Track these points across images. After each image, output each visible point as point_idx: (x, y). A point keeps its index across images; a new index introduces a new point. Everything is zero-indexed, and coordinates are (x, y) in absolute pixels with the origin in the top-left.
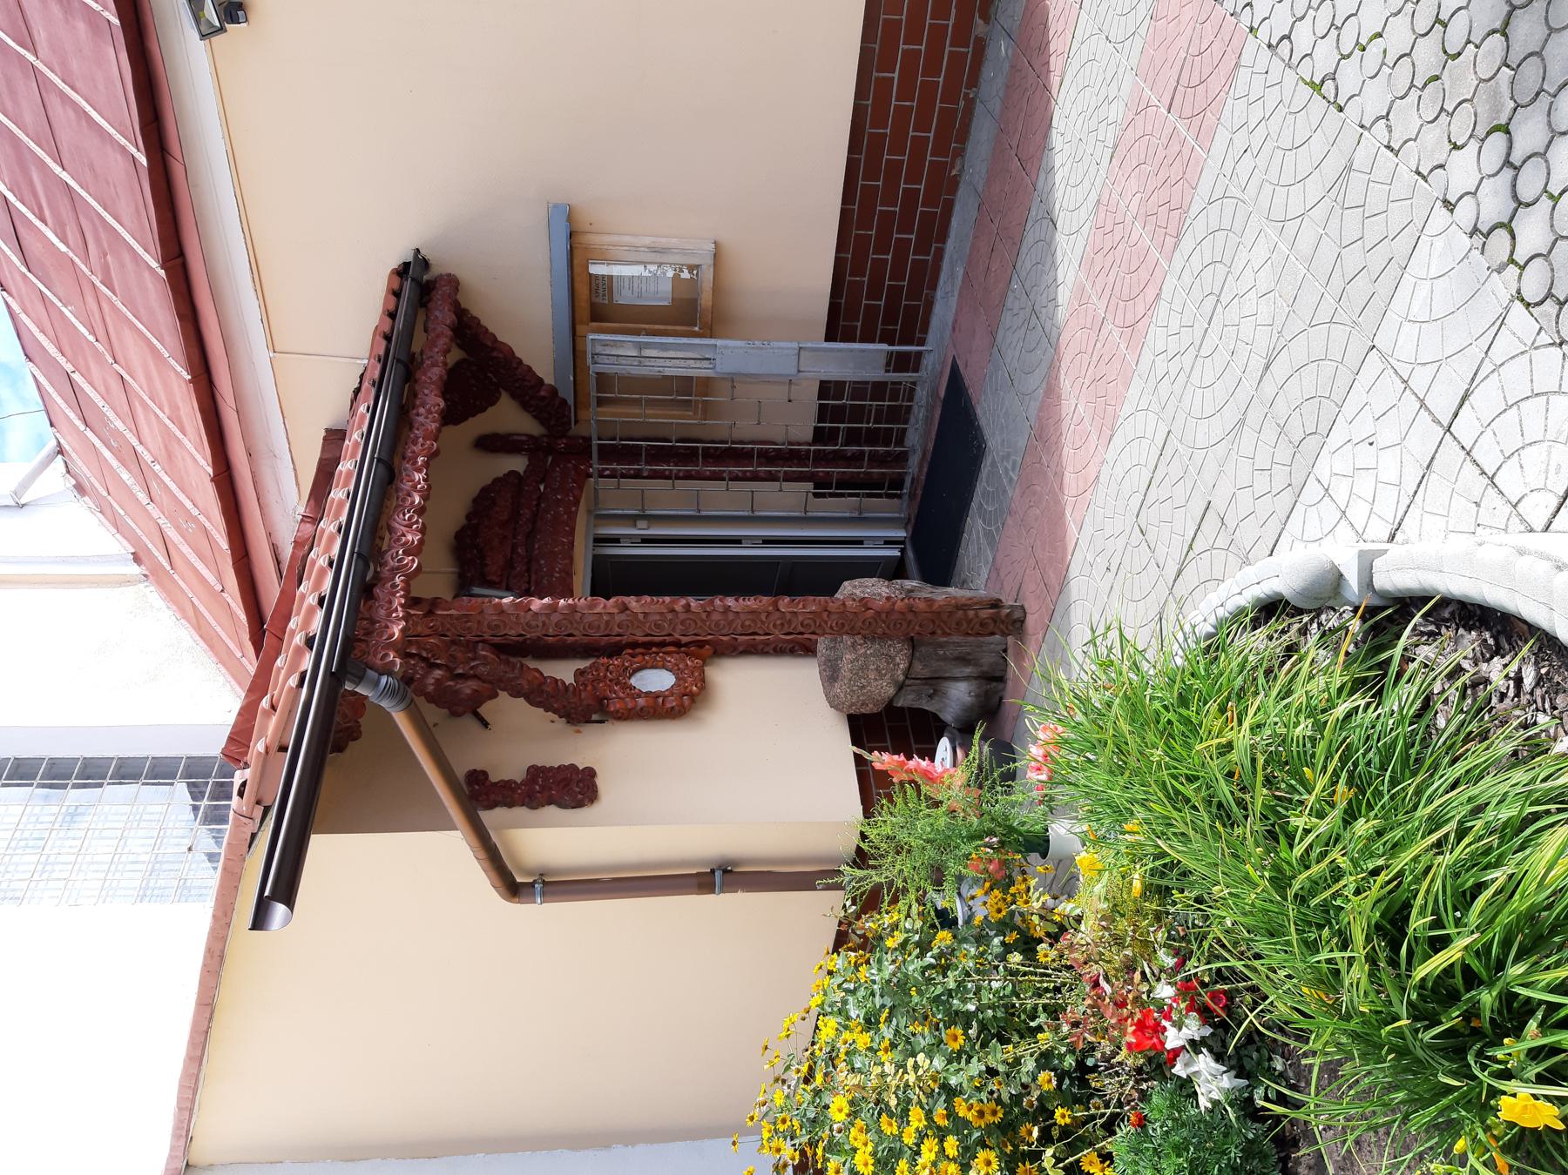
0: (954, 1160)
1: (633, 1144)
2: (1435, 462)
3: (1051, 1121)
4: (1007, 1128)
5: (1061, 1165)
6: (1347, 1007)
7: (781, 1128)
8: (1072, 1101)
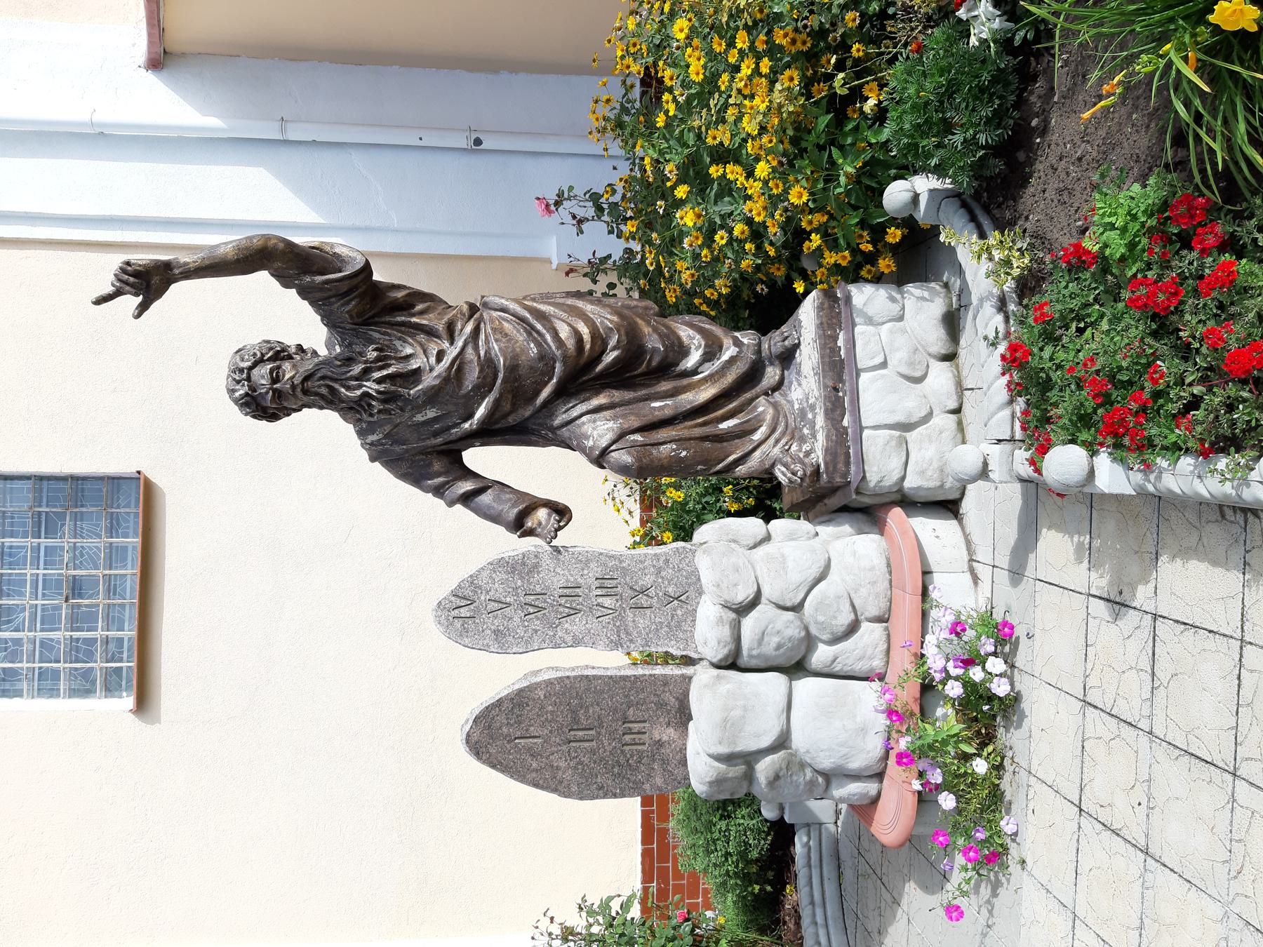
0: (765, 76)
1: (516, 73)
2: (1151, 679)
3: (847, 55)
4: (811, 57)
5: (847, 86)
6: (1111, 28)
7: (632, 50)
8: (868, 41)
